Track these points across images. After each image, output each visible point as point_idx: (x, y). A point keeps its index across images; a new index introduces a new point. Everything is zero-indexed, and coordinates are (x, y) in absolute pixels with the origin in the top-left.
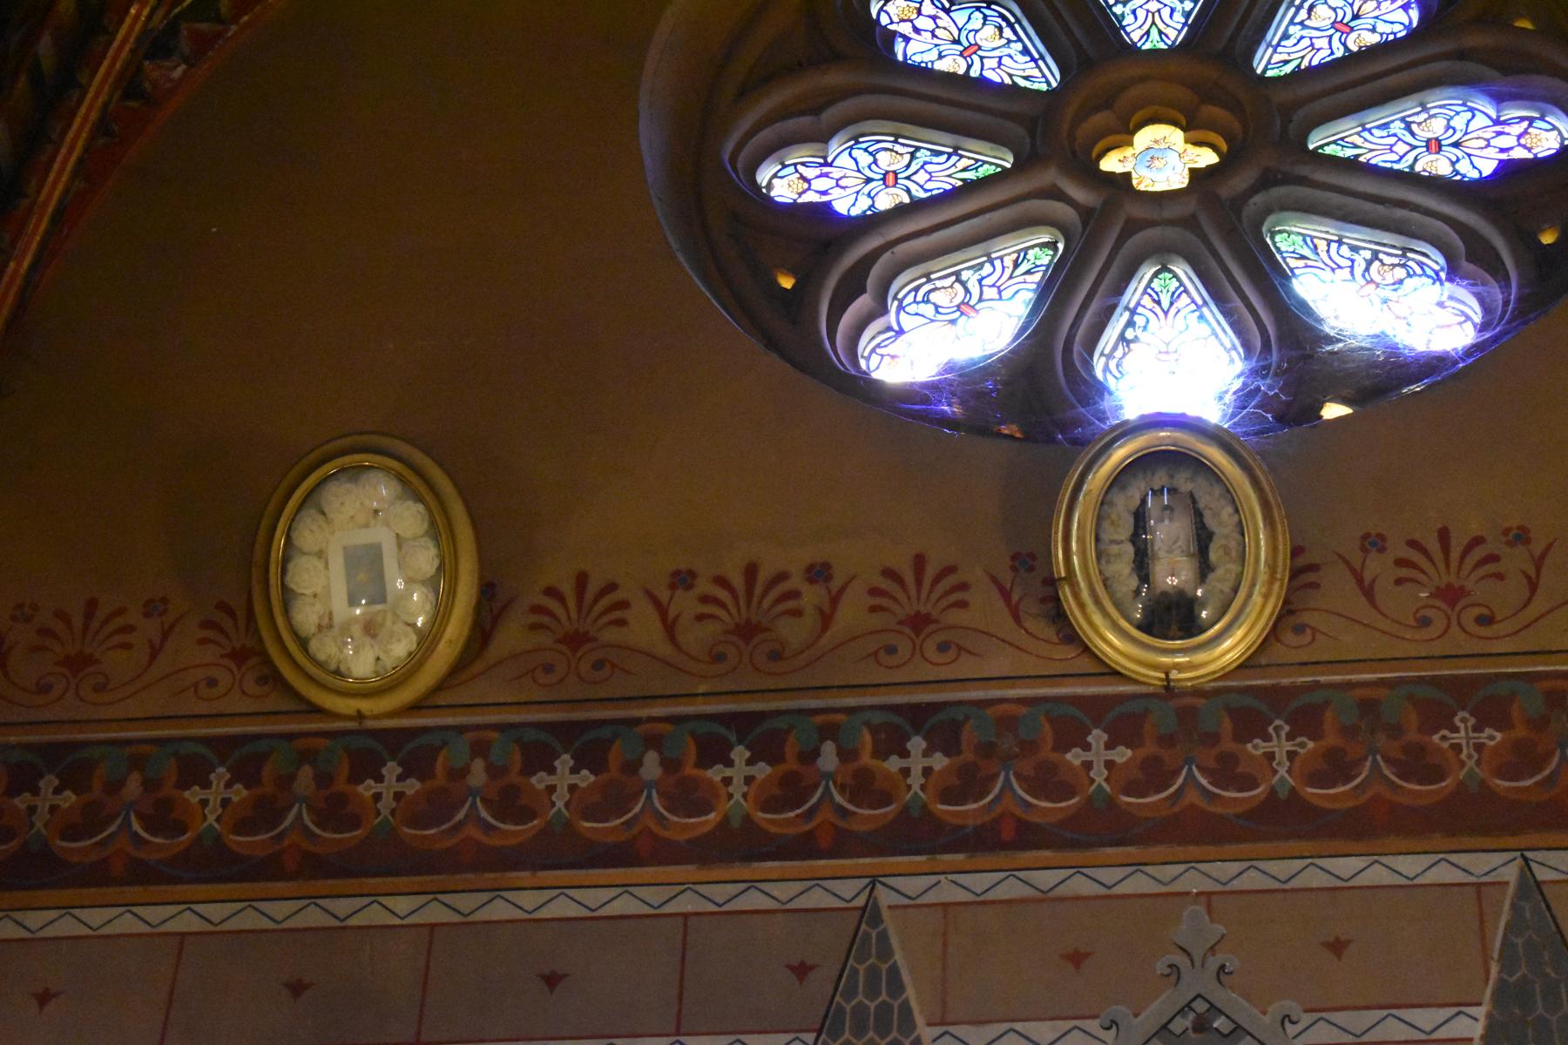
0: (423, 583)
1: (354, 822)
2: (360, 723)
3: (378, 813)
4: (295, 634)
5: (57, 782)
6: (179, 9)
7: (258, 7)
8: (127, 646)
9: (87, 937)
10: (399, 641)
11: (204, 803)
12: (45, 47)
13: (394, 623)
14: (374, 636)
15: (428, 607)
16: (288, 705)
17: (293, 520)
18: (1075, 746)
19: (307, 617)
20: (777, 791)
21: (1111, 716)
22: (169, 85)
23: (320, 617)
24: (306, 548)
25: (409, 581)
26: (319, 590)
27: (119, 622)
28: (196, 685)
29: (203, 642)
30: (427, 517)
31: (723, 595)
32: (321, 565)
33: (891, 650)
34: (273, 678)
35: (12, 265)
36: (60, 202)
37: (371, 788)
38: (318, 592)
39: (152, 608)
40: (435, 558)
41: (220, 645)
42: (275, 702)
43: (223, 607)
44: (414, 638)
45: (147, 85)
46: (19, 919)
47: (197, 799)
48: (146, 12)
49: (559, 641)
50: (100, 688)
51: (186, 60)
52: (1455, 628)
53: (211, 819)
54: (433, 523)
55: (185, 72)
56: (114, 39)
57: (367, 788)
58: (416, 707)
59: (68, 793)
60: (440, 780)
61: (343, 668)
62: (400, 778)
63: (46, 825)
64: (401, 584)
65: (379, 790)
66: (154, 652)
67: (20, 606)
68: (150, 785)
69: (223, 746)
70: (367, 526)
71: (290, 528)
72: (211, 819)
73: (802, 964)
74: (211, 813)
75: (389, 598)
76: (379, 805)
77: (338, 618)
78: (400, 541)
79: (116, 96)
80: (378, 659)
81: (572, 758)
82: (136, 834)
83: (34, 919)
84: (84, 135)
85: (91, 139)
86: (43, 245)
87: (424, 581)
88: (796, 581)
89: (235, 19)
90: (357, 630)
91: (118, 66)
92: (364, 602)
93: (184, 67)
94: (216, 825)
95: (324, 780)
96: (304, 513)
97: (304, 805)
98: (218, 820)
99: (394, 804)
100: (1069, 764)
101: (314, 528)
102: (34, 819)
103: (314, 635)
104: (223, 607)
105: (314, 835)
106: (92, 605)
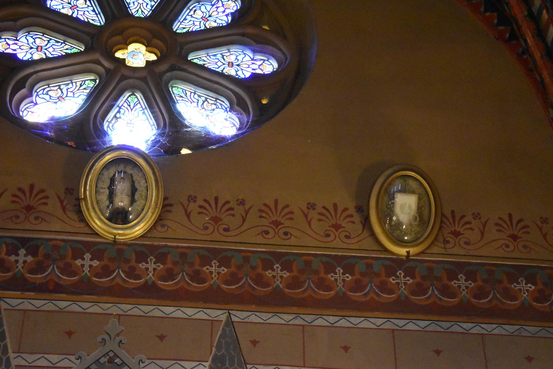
33: (17, 217)
94: (22, 270)
99: (23, 265)
106: (32, 187)
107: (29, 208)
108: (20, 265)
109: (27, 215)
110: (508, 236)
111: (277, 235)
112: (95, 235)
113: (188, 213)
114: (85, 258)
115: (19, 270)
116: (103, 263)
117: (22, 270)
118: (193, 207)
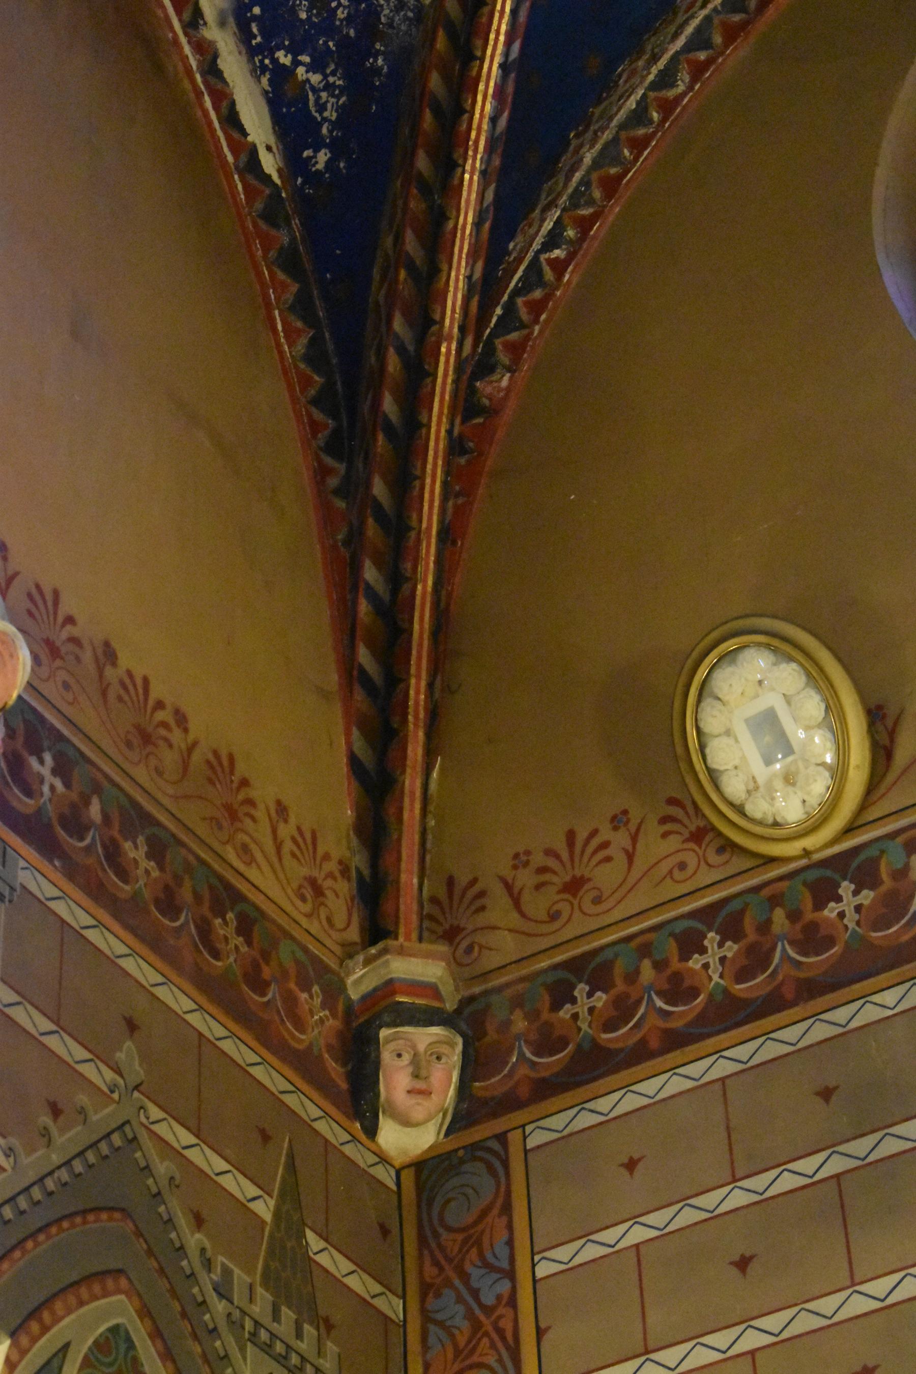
0: (819, 726)
1: (830, 941)
2: (809, 859)
3: (846, 927)
4: (731, 804)
5: (587, 988)
6: (488, 331)
7: (551, 303)
8: (608, 859)
9: (649, 1105)
10: (815, 781)
11: (706, 966)
12: (389, 405)
13: (806, 768)
14: (794, 784)
15: (829, 745)
16: (749, 863)
17: (697, 712)
18: (829, 901)
19: (734, 787)
20: (745, 962)
21: (719, 920)
22: (502, 394)
23: (746, 784)
24: (716, 731)
25: (807, 728)
26: (737, 762)
27: (595, 843)
28: (671, 872)
29: (665, 835)
30: (802, 672)
31: (551, 863)
32: (731, 741)
33: (682, 866)
34: (728, 847)
35: (419, 587)
36: (441, 521)
37: (835, 909)
38: (737, 764)
39: (618, 820)
40: (821, 703)
41: (680, 833)
42: (739, 863)
43: (672, 801)
44: (827, 774)
45: (486, 402)
46: (592, 1108)
47: (835, 913)
48: (454, 346)
49: (686, 841)
50: (597, 901)
51: (509, 369)
52: (577, 913)
53: (716, 978)
54: (808, 675)
55: (511, 379)
56: (436, 378)
57: (831, 911)
58: (849, 830)
59: (599, 994)
60: (888, 883)
61: (779, 819)
62: (856, 893)
63: (590, 1026)
64: (801, 733)
65: (841, 909)
66: (630, 857)
67: (516, 856)
68: (660, 966)
69: (707, 914)
70: (757, 696)
71: (696, 720)
72: (716, 978)
73: (631, 1159)
74: (714, 972)
75: (796, 748)
76: (846, 921)
77: (761, 781)
78: (788, 699)
79: (458, 421)
80: (804, 801)
81: (716, 933)
82: (661, 1010)
83: (604, 1104)
84: (440, 462)
85: (448, 464)
86: (438, 562)
87: (819, 724)
88: (606, 833)
89: (536, 321)
90: (779, 784)
91: (447, 397)
92: (780, 756)
93: (508, 375)
94: (722, 982)
95: (794, 916)
96: (702, 704)
97: (786, 942)
98: (721, 977)
99: (857, 917)
100: (827, 919)
101: (715, 713)
102: (579, 1023)
103: (746, 800)
104: (672, 801)
105: (800, 963)
106: (571, 836)
107: (574, 886)
108: (851, 920)
109: (576, 902)
110: (559, 892)
111: (702, 863)
112: (769, 865)
113: (515, 896)
114: (576, 998)
115: (586, 1031)
116: (744, 942)
117: (722, 982)
118: (525, 879)
